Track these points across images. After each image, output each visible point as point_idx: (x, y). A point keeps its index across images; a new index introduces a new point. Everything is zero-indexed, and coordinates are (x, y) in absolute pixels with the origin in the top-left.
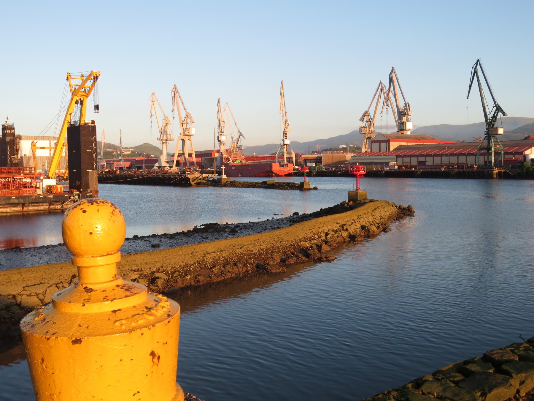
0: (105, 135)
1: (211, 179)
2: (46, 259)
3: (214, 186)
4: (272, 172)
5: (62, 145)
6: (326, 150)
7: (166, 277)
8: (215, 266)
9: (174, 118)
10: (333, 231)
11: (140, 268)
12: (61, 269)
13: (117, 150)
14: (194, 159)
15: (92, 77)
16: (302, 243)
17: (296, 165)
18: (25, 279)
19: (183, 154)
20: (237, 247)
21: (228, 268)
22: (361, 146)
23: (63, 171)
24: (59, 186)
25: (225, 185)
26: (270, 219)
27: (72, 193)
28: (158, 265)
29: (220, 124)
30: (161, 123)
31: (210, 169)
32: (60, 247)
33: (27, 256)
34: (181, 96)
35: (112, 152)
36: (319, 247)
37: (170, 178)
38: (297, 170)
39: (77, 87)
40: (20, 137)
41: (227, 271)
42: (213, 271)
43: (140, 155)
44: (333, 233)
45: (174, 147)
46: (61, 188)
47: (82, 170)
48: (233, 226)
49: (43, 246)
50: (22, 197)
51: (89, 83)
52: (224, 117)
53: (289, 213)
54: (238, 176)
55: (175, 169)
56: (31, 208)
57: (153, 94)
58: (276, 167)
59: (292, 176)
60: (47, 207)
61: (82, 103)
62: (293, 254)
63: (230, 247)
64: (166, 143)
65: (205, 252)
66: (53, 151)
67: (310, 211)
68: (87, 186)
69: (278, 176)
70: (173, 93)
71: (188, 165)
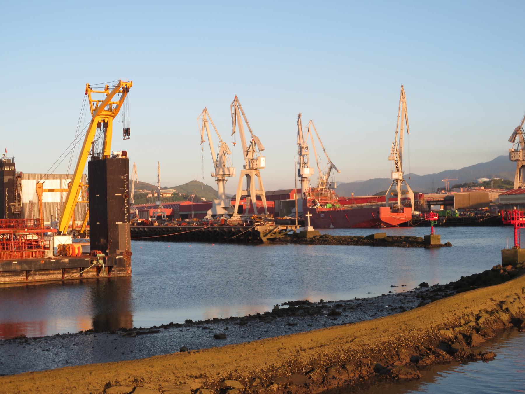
0: (140, 173)
1: (291, 233)
2: (63, 355)
3: (295, 242)
4: (380, 221)
5: (77, 187)
6: (459, 186)
7: (242, 387)
8: (314, 370)
9: (234, 144)
10: (487, 312)
11: (203, 373)
12: (91, 373)
13: (152, 191)
14: (265, 203)
15: (121, 90)
16: (442, 332)
17: (416, 210)
18: (40, 389)
19: (249, 196)
20: (345, 340)
21: (333, 372)
22: (511, 179)
23: (79, 223)
24: (76, 246)
25: (312, 242)
26: (387, 293)
27: (95, 255)
28: (230, 368)
29: (301, 152)
30: (217, 151)
31: (288, 218)
32: (82, 337)
33: (37, 350)
34: (245, 112)
35: (149, 194)
36: (468, 339)
37: (230, 231)
38: (416, 216)
39: (100, 104)
40: (20, 176)
41: (331, 377)
42: (310, 378)
43: (185, 198)
44: (487, 316)
45: (235, 186)
46: (79, 248)
47: (109, 223)
48: (331, 305)
49: (58, 335)
50: (26, 262)
51: (116, 98)
52: (308, 141)
53: (413, 285)
54: (329, 228)
55: (236, 217)
56: (37, 278)
57: (205, 110)
58: (385, 214)
59: (410, 226)
60: (60, 276)
61: (106, 125)
62: (430, 350)
63: (336, 341)
64: (223, 180)
65: (298, 348)
66: (65, 194)
67: (444, 281)
68: (116, 246)
69: (389, 226)
70: (233, 108)
71: (256, 213)
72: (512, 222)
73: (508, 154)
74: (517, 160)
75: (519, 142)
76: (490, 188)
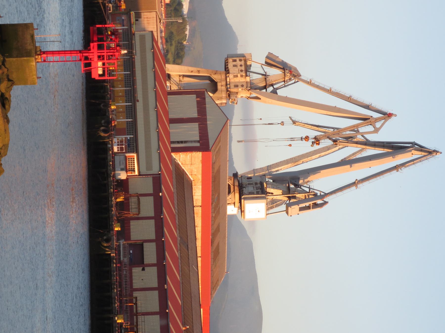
22: (186, 59)
72: (94, 45)
73: (239, 52)
74: (227, 71)
75: (265, 75)
76: (168, 15)
